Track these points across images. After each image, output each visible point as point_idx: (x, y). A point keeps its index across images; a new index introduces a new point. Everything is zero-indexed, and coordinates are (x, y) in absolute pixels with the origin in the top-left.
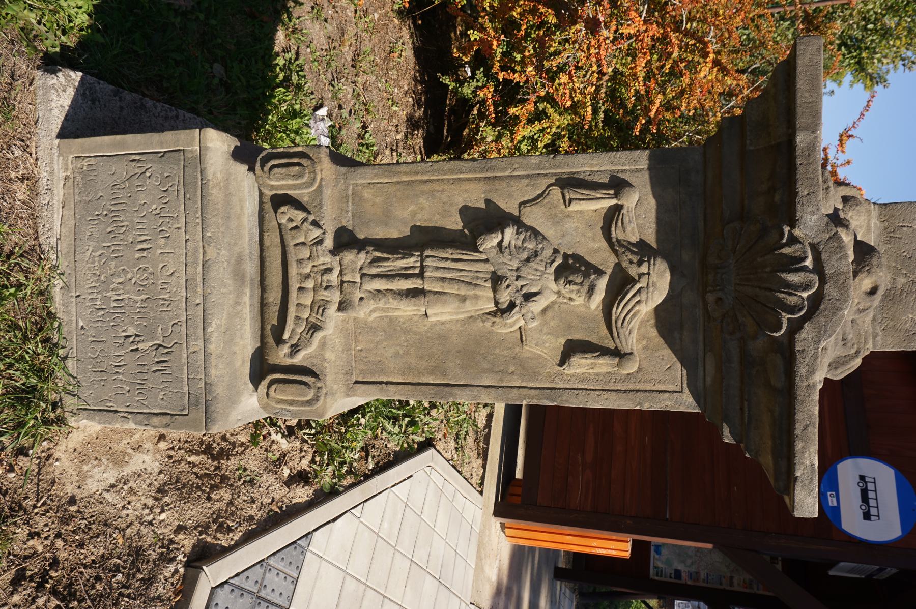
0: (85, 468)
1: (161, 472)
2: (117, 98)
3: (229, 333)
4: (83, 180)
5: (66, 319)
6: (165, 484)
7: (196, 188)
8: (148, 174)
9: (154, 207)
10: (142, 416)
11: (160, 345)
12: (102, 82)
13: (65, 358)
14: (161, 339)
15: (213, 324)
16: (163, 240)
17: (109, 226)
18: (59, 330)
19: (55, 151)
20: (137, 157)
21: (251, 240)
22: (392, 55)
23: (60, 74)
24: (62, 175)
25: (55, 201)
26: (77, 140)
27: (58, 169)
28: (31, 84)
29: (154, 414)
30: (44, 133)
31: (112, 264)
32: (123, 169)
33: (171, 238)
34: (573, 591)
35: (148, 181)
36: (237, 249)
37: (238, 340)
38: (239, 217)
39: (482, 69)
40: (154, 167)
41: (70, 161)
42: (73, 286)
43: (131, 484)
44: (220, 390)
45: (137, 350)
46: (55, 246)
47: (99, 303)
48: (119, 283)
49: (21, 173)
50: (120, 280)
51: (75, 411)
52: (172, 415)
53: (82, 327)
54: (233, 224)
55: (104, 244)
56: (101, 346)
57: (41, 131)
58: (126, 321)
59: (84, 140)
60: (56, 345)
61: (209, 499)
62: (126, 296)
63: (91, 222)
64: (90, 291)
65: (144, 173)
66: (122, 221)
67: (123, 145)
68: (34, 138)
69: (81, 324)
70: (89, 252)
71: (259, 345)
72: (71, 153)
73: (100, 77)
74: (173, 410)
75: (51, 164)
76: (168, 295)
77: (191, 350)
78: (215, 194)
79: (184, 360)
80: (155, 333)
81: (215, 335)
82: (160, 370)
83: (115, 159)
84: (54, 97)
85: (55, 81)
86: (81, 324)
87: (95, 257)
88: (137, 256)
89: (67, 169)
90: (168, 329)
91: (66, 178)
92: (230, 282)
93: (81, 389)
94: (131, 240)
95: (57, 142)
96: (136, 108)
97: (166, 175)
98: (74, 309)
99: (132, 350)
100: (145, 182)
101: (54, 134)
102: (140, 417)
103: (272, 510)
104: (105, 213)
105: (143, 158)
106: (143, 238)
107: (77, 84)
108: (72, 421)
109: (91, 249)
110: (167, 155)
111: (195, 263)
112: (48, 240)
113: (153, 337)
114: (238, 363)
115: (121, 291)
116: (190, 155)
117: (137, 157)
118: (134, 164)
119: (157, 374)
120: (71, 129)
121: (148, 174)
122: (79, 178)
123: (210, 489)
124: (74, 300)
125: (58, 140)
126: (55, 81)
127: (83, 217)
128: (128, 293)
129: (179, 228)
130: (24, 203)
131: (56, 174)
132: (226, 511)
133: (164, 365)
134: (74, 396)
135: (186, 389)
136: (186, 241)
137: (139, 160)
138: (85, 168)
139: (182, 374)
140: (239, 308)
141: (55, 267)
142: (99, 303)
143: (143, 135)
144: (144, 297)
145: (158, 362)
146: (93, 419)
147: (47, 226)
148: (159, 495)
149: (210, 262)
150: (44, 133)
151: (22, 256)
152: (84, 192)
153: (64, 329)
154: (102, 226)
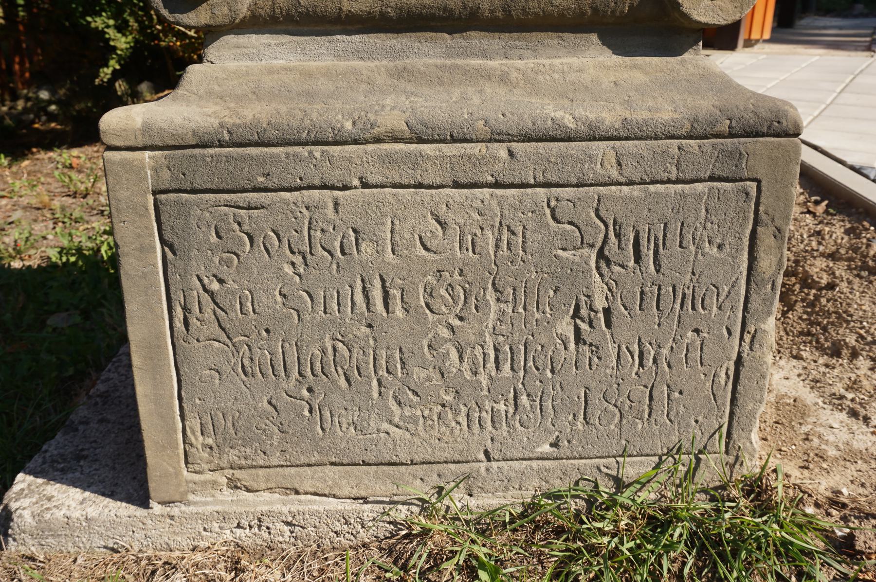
0: (832, 452)
1: (798, 357)
2: (81, 428)
3: (568, 93)
4: (239, 448)
5: (536, 483)
6: (820, 348)
7: (243, 159)
8: (215, 286)
9: (288, 269)
10: (754, 297)
11: (601, 255)
12: (45, 447)
13: (620, 484)
14: (586, 251)
15: (558, 114)
16: (363, 246)
17: (334, 383)
18: (559, 497)
19: (175, 510)
20: (179, 312)
21: (358, 54)
22: (74, 165)
23: (13, 506)
24: (227, 494)
25: (285, 510)
26: (150, 460)
27: (216, 502)
28: (33, 559)
29: (750, 269)
30: (139, 535)
31: (418, 374)
32: (207, 351)
33: (360, 225)
34: (801, 18)
35: (231, 285)
36: (381, 79)
37: (586, 78)
38: (308, 75)
39: (89, 19)
40: (200, 265)
41: (196, 477)
42: (464, 468)
43: (839, 389)
44: (705, 104)
45: (607, 312)
46: (379, 508)
47: (502, 407)
48: (461, 358)
49: (223, 573)
50: (454, 355)
51: (731, 459)
52: (756, 222)
53: (554, 445)
54: (324, 85)
55: (376, 395)
56: (596, 399)
57: (135, 542)
58: (543, 339)
59: (148, 444)
60: (590, 502)
61: (831, 286)
62: (489, 341)
63: (327, 426)
64: (476, 427)
65: (211, 294)
66: (324, 351)
67: (154, 350)
68: (150, 553)
69: (546, 448)
70: (393, 430)
71: (594, 37)
72: (178, 474)
73: (37, 448)
74: (745, 218)
75: (205, 518)
76: (488, 233)
77: (615, 174)
78: (255, 113)
79: (636, 191)
80: (572, 266)
81: (580, 112)
82: (656, 253)
83: (184, 369)
84: (59, 514)
85: (27, 514)
86: (546, 448)
87: (402, 417)
88: (399, 313)
89: (214, 484)
90: (564, 231)
91: (234, 485)
92: (456, 94)
93: (686, 444)
94: (365, 330)
95: (156, 508)
96: (104, 403)
97: (214, 239)
98: (516, 464)
99: (608, 324)
100: (233, 293)
101: (140, 512)
102: (754, 305)
103: (826, 212)
104: (305, 393)
105: (178, 297)
106: (359, 297)
107: (40, 481)
108: (751, 467)
109: (386, 426)
110: (169, 236)
111: (417, 160)
112: (370, 522)
113: (578, 271)
114: (639, 77)
115: (478, 351)
116: (166, 175)
117: (179, 312)
118: (193, 321)
119: (663, 260)
120: (124, 474)
121: (215, 286)
122: (232, 456)
123: (811, 288)
124: (494, 465)
125: (153, 503)
126: (27, 514)
127: (316, 447)
128: (481, 334)
129: (336, 205)
130: (289, 569)
131: (226, 508)
132: (850, 260)
133: (644, 242)
134: (698, 460)
135: (700, 187)
136: (365, 185)
137: (185, 309)
138: (210, 441)
139: (668, 196)
140: (514, 75)
141: (425, 506)
142: (502, 407)
143: (128, 297)
144: (491, 296)
145: (638, 258)
146: (752, 415)
147: (338, 527)
148: (845, 352)
149: (413, 122)
150: (139, 535)
151: (404, 568)
152: (262, 442)
153: (557, 485)
154: (336, 399)
